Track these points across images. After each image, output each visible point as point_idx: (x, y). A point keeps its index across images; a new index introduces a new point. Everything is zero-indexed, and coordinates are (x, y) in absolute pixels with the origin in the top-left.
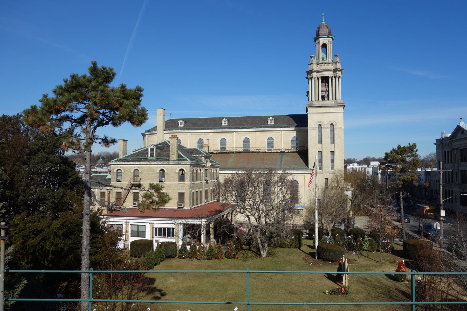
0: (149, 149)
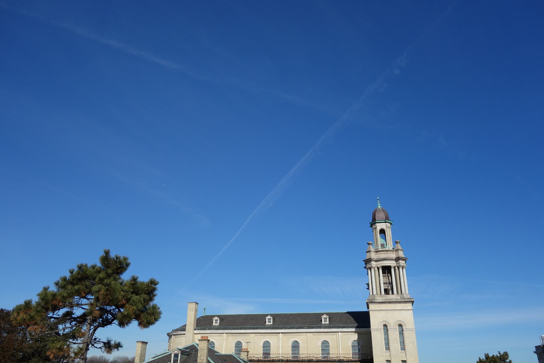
0: (173, 355)
